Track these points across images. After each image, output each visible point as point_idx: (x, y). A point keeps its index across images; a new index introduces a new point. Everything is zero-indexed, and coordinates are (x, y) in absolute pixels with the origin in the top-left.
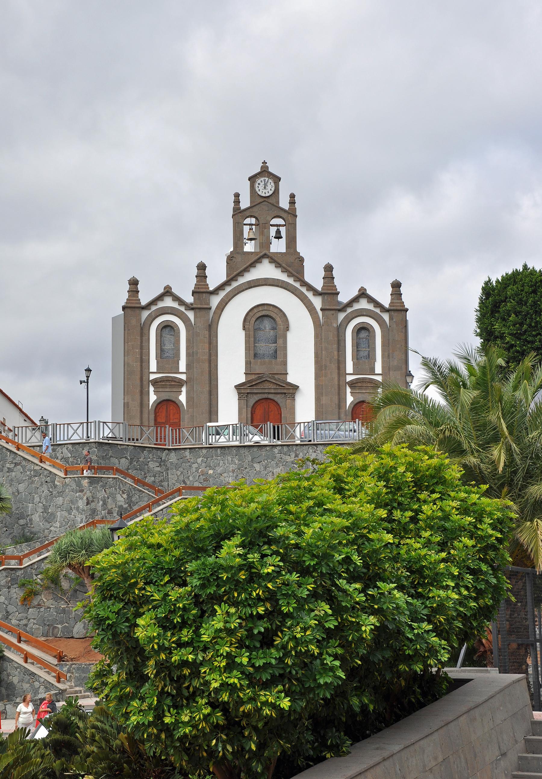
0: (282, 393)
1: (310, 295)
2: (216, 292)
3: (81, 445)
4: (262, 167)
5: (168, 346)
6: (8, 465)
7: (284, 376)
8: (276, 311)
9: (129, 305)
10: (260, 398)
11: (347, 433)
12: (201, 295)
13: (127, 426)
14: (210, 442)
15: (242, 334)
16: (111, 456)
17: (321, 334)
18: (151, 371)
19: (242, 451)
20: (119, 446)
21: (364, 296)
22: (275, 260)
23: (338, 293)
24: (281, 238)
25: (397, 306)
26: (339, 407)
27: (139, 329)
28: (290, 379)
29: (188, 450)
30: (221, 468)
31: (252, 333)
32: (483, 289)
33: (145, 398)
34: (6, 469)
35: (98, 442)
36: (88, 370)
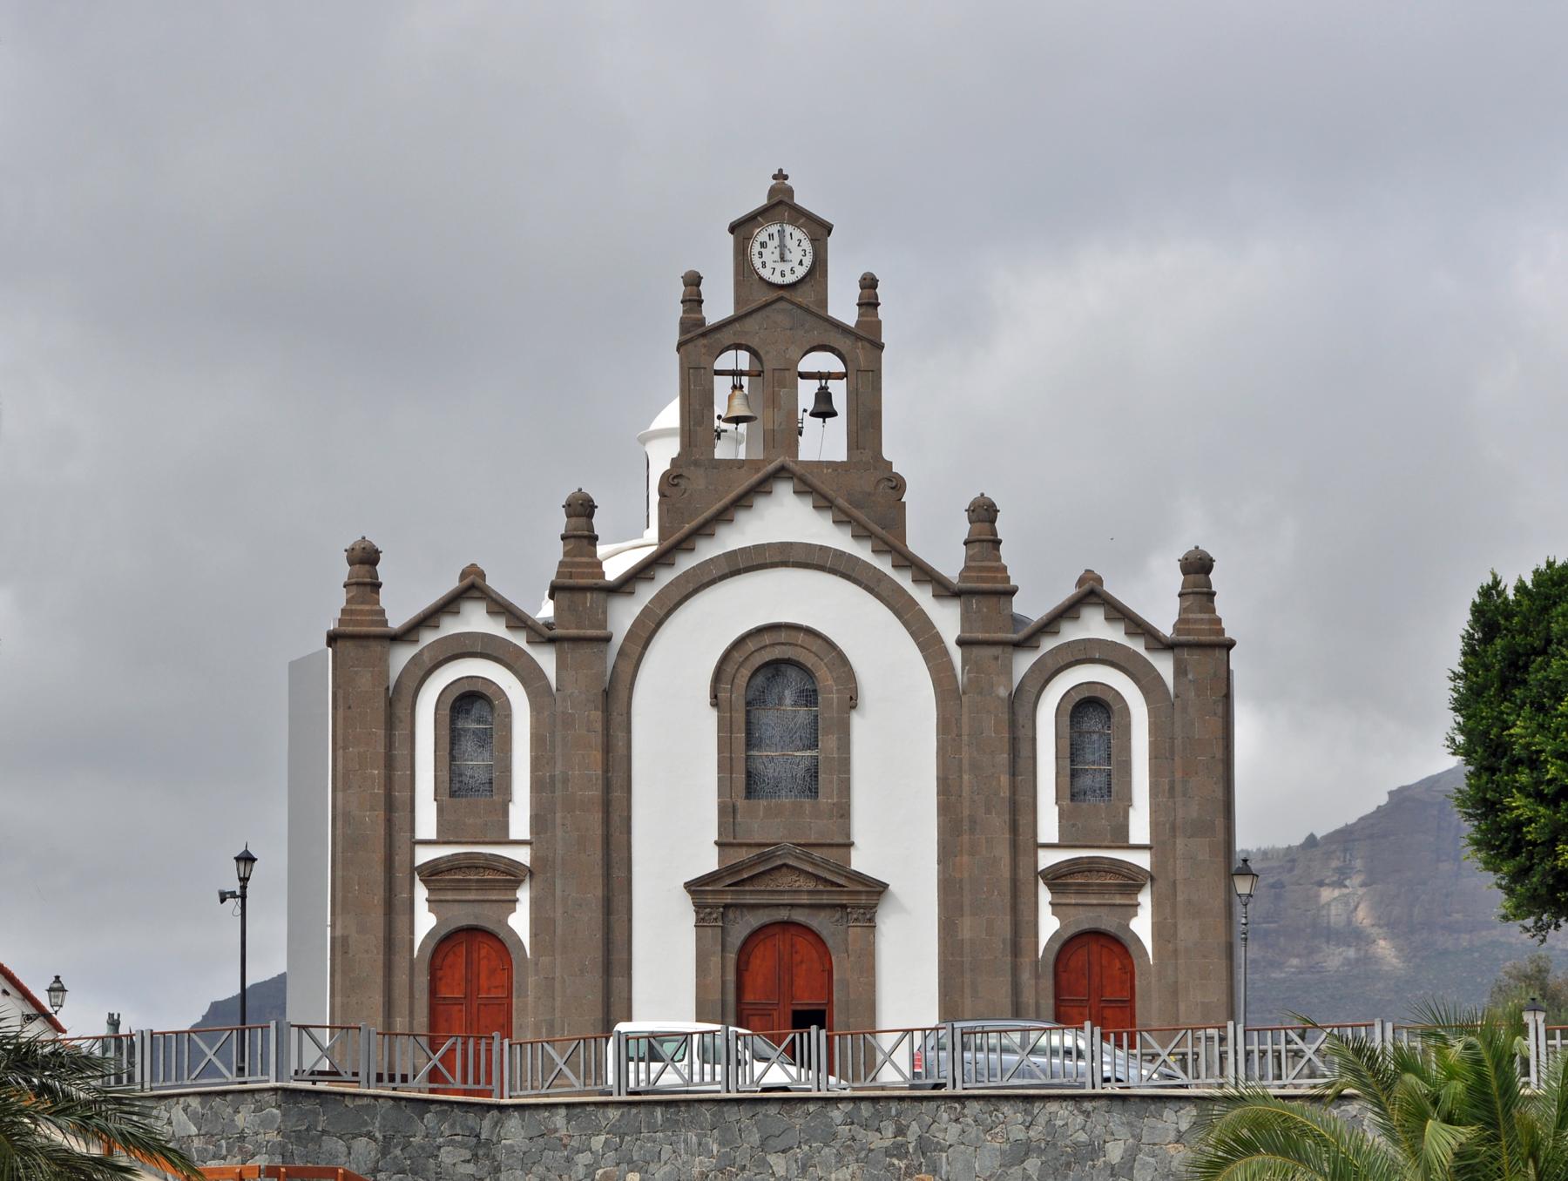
0: (833, 906)
1: (923, 597)
3: (229, 1098)
4: (772, 192)
5: (475, 762)
7: (842, 851)
9: (350, 629)
11: (1056, 1061)
12: (578, 596)
14: (632, 1084)
15: (707, 722)
16: (324, 1132)
17: (958, 721)
18: (420, 835)
19: (732, 1114)
20: (348, 1101)
21: (1095, 600)
22: (815, 486)
23: (1012, 592)
24: (834, 414)
25: (1200, 632)
26: (1016, 950)
27: (381, 704)
28: (861, 861)
29: (563, 1111)
30: (667, 1168)
31: (740, 717)
32: (1477, 610)
33: (400, 922)
35: (285, 1090)
36: (246, 859)
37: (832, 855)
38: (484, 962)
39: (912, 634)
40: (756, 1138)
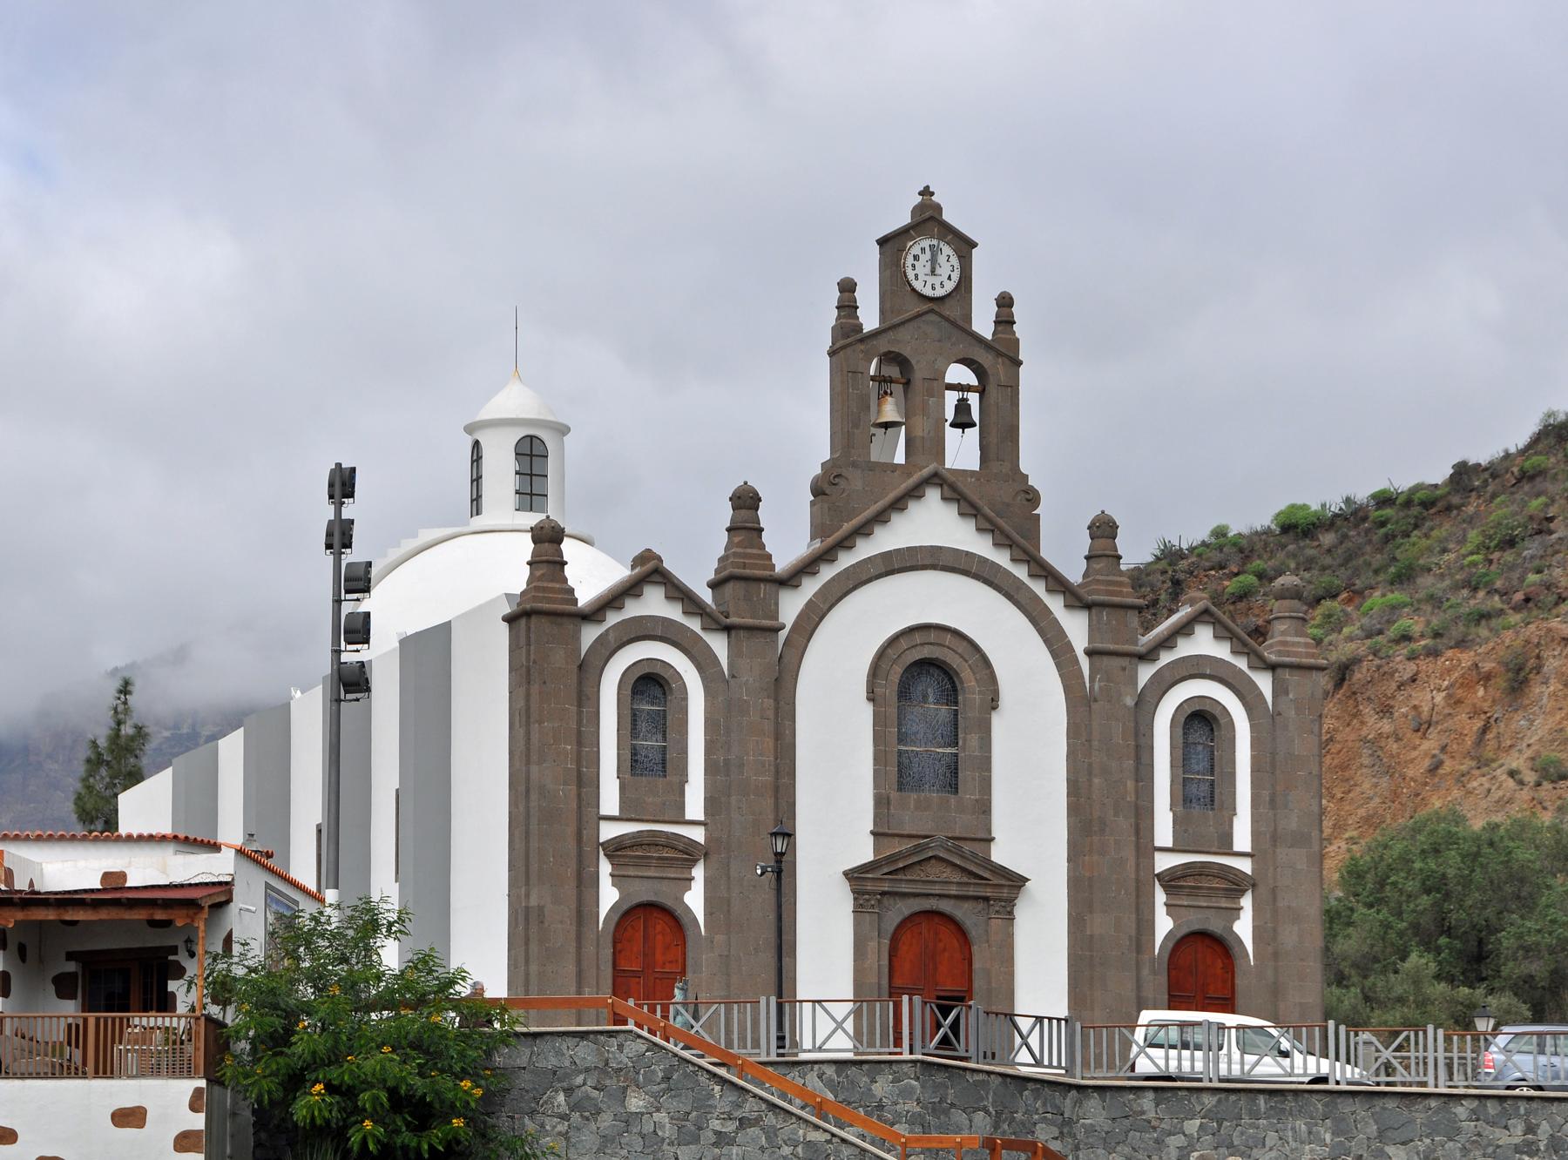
0: (976, 898)
1: (1055, 604)
2: (791, 580)
3: (865, 1067)
4: (917, 210)
6: (715, 1124)
8: (962, 647)
10: (917, 909)
12: (754, 585)
13: (981, 1014)
15: (864, 714)
16: (952, 1105)
19: (1346, 1106)
22: (955, 490)
25: (1296, 654)
26: (1139, 950)
28: (1000, 854)
29: (1151, 1095)
31: (893, 711)
34: (708, 1136)
37: (977, 848)
38: (659, 937)
39: (1046, 641)
40: (1373, 1129)
